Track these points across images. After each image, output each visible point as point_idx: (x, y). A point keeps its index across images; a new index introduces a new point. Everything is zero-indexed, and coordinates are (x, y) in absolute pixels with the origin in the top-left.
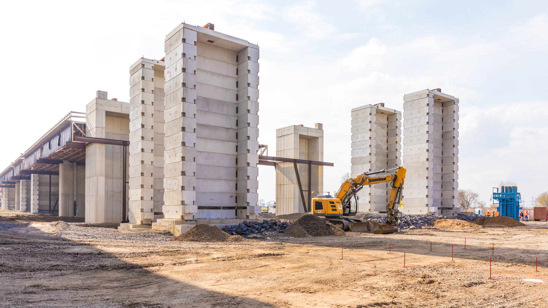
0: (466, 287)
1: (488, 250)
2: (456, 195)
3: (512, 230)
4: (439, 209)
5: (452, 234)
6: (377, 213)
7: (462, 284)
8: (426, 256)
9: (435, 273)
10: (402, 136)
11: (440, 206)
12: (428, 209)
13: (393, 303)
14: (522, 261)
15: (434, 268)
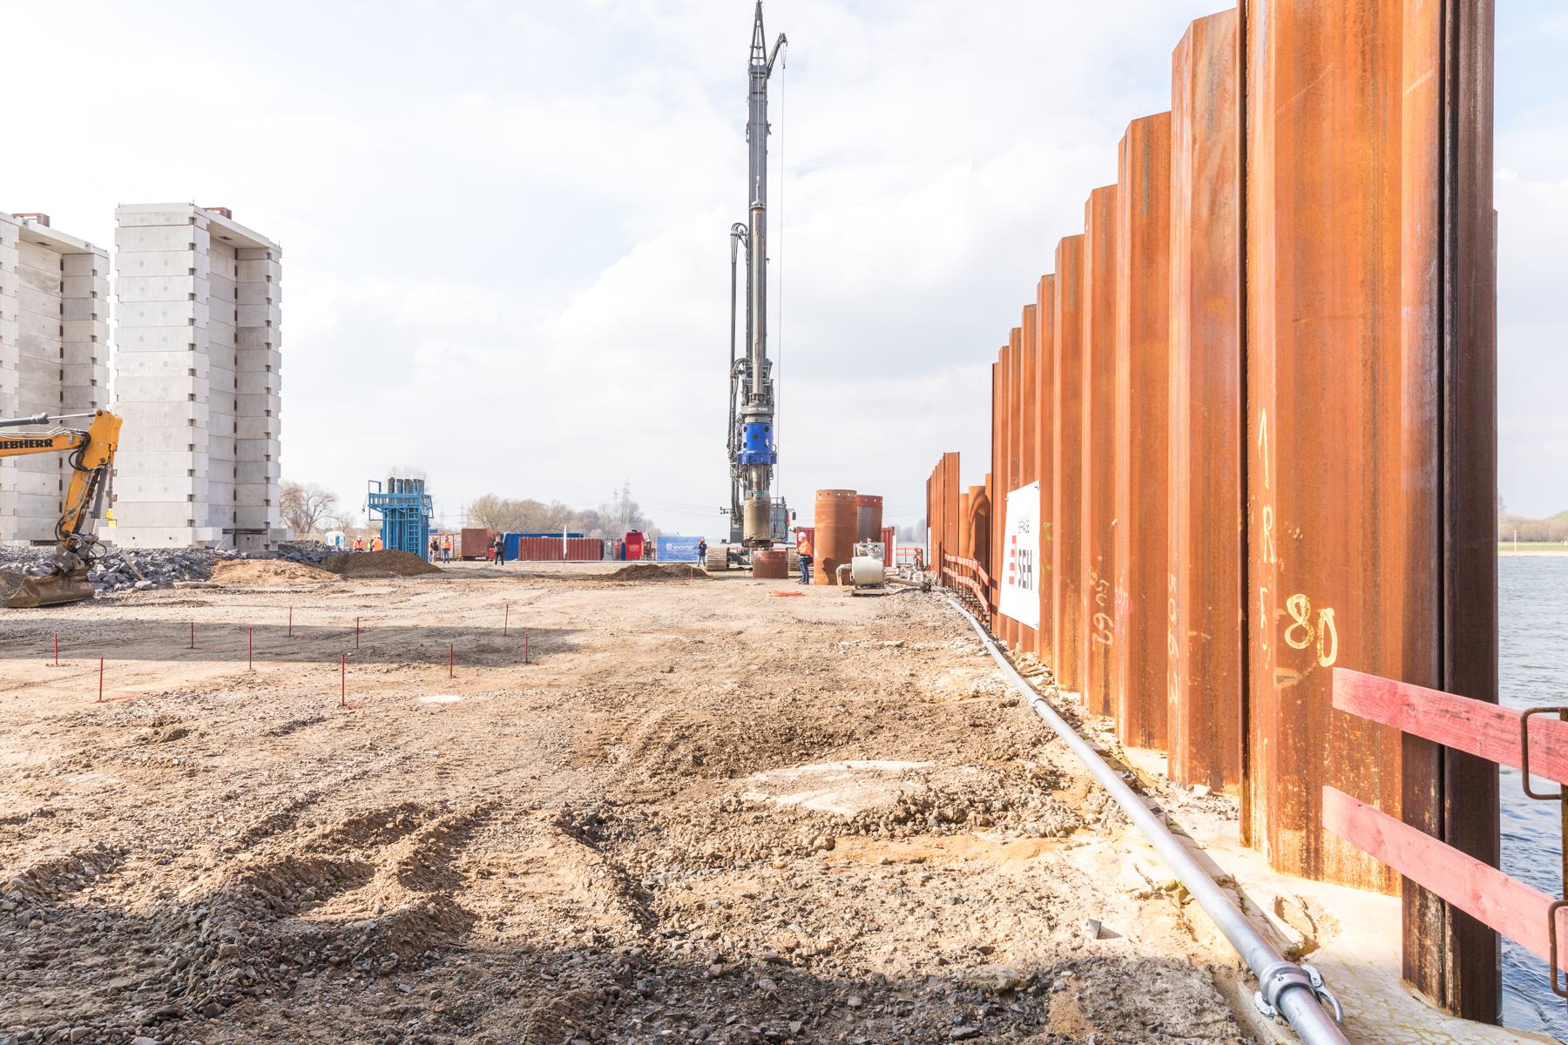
0: (276, 734)
1: (348, 634)
2: (275, 496)
3: (410, 583)
4: (225, 532)
5: (259, 599)
6: (25, 544)
7: (267, 728)
8: (175, 663)
9: (194, 709)
10: (112, 322)
11: (230, 525)
12: (195, 534)
13: (42, 813)
14: (424, 657)
15: (191, 696)
